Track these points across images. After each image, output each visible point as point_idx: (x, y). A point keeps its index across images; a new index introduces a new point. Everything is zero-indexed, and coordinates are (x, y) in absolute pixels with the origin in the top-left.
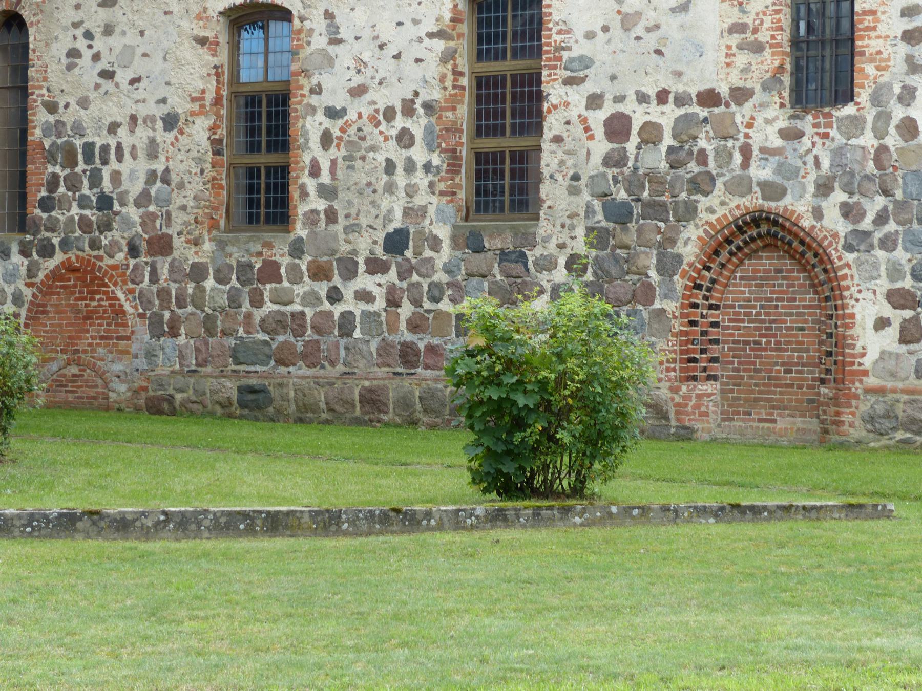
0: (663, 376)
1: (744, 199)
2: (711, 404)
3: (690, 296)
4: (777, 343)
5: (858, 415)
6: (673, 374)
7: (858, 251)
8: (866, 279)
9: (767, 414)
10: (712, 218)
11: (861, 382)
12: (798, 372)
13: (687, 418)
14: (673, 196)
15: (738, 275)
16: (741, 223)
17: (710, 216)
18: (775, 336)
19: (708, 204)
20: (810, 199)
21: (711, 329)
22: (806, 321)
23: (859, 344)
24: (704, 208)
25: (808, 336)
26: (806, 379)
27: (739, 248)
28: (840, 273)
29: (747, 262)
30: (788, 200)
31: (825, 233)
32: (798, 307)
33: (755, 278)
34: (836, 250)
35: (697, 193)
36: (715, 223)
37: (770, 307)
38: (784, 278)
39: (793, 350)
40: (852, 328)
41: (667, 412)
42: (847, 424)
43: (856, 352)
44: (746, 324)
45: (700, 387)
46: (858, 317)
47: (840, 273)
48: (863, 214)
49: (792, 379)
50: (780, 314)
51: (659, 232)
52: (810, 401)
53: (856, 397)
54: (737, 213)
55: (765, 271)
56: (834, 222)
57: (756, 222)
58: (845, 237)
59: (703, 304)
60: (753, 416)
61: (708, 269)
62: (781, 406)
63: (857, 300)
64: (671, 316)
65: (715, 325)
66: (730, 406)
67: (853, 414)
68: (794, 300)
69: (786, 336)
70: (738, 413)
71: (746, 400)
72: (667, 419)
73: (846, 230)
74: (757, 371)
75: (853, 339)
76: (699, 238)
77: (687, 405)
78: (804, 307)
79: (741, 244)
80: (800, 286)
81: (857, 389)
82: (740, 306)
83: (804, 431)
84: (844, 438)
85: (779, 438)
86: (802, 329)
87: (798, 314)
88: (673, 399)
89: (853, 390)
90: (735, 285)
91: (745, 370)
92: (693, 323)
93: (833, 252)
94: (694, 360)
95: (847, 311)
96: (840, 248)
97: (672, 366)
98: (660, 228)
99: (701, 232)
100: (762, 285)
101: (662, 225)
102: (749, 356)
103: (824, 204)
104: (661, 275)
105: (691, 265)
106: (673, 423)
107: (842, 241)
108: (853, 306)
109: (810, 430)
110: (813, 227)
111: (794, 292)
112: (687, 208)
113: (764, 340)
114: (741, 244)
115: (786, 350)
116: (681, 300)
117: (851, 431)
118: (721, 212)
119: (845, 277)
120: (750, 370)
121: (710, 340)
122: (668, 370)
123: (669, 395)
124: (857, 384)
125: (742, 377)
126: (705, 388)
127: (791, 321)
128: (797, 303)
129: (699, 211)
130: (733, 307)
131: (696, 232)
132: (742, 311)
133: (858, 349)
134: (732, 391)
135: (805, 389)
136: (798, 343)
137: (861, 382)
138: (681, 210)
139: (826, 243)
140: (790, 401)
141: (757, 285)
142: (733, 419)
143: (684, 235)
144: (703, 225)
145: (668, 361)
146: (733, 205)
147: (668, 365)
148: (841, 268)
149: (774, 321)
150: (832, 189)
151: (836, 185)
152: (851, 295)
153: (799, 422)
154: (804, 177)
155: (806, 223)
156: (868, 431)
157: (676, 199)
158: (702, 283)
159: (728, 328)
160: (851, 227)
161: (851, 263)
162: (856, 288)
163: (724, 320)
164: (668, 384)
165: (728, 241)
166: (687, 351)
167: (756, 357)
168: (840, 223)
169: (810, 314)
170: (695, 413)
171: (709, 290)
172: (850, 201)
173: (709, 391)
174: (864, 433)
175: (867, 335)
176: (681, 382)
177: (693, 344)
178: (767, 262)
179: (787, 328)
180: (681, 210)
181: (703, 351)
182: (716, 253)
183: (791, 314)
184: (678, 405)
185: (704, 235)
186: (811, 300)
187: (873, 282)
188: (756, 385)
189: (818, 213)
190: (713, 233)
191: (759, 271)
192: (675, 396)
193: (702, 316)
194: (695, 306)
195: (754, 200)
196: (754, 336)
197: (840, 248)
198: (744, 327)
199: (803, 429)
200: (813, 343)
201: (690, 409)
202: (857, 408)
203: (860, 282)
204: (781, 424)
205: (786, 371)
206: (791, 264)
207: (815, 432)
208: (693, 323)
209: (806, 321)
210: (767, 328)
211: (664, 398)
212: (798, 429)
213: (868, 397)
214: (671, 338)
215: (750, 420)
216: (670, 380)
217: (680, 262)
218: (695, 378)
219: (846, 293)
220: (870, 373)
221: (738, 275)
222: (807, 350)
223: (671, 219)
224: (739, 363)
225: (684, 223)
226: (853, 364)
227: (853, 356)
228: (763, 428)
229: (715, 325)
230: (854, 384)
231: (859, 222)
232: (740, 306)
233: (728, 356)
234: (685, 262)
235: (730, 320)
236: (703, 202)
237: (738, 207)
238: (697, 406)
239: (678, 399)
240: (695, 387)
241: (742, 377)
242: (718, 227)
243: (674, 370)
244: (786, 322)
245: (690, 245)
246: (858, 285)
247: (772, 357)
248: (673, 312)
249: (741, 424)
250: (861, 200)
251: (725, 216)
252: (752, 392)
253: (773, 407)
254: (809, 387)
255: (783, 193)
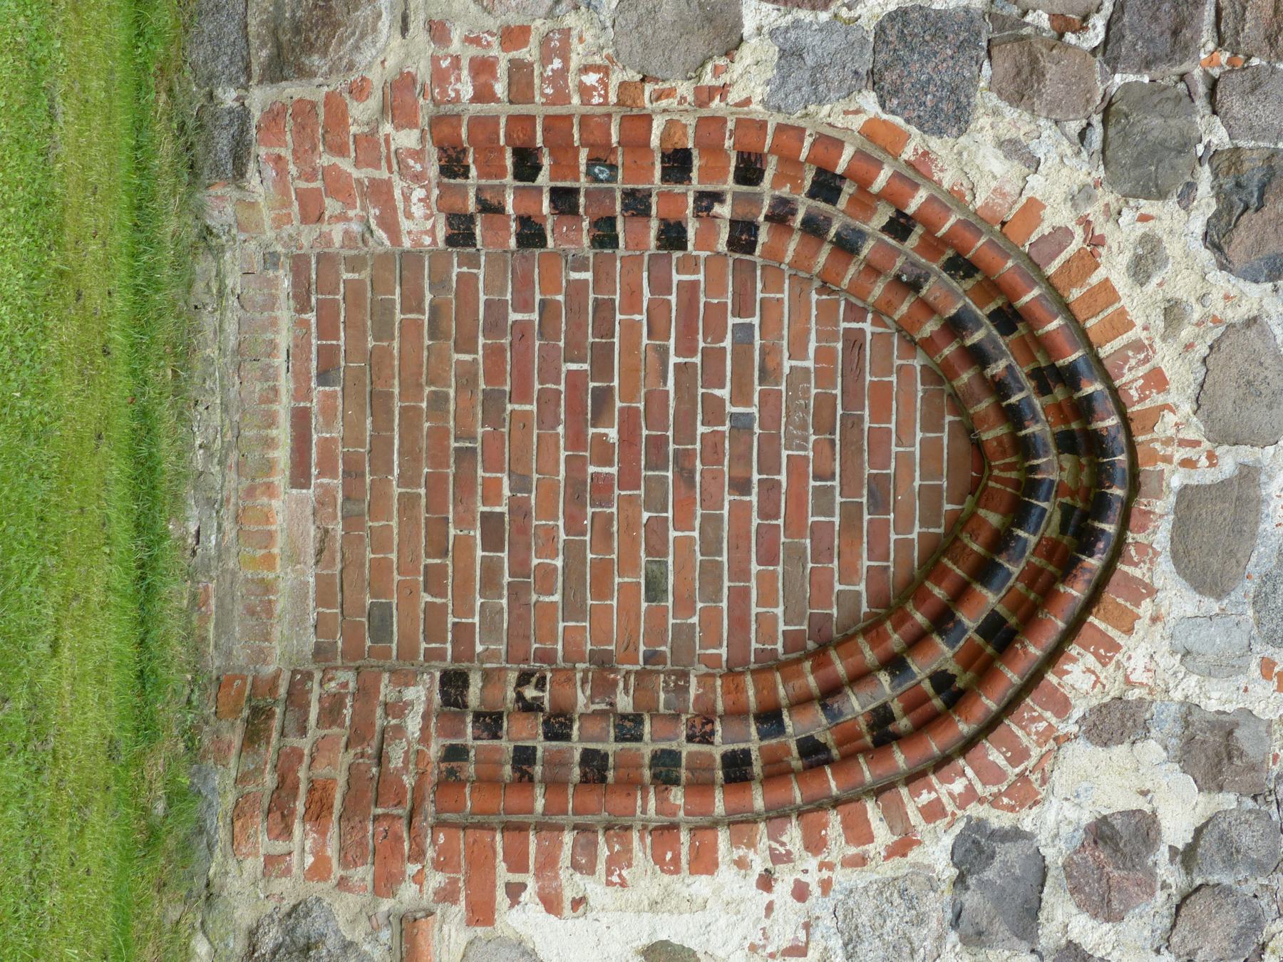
0: (456, 46)
1: (1187, 408)
2: (356, 227)
3: (789, 161)
4: (602, 488)
5: (318, 888)
6: (467, 91)
7: (960, 882)
8: (849, 914)
9: (326, 444)
10: (1113, 268)
11: (447, 895)
12: (491, 570)
13: (287, 153)
14: (1213, 85)
15: (868, 327)
16: (1088, 389)
17: (1125, 259)
18: (629, 478)
19: (1173, 248)
20: (1178, 695)
21: (654, 225)
22: (684, 605)
23: (593, 887)
24: (1158, 228)
25: (629, 610)
26: (464, 606)
27: (978, 357)
28: (872, 810)
29: (917, 363)
30: (1176, 598)
31: (1035, 752)
32: (740, 572)
33: (852, 395)
34: (970, 795)
35: (1218, 192)
36: (1095, 279)
37: (741, 458)
38: (851, 515)
39: (574, 553)
40: (659, 860)
41: (303, 73)
42: (280, 847)
43: (564, 874)
44: (673, 360)
45: (419, 193)
46: (701, 885)
47: (872, 810)
48: (1105, 907)
49: (464, 545)
50: (711, 501)
51: (1063, 25)
52: (380, 623)
53: (386, 884)
54: (1131, 378)
55: (879, 440)
56: (1081, 785)
57: (1084, 443)
58: (1015, 835)
59: (756, 200)
60: (317, 391)
61: (900, 226)
62: (358, 505)
63: (766, 882)
64: (708, 79)
65: (673, 236)
66: (355, 290)
67: (319, 871)
68: (768, 558)
69: (630, 525)
70: (327, 329)
71: (377, 361)
72: (278, 70)
73: (1043, 838)
74: (493, 401)
75: (612, 862)
76: (1033, 209)
77: (341, 151)
78: (740, 597)
79: (998, 368)
80: (820, 583)
81: (419, 879)
82: (744, 332)
83: (261, 611)
84: (222, 835)
85: (228, 513)
86: (655, 589)
87: (711, 573)
88: (359, 90)
89: (412, 868)
90: (827, 313)
91: (494, 354)
92: (677, 164)
93: (958, 786)
94: (526, 165)
95: (723, 836)
96: (975, 810)
97: (500, 88)
98: (1082, 25)
99: (1057, 215)
100: (823, 426)
101: (1096, 34)
102: (549, 373)
103: (1151, 750)
104: (881, 30)
105: (919, 170)
106: (260, 98)
107: (999, 819)
108: (741, 864)
109: (266, 637)
110: (1062, 706)
111: (796, 555)
112: (1156, 152)
113: (613, 434)
114: (998, 368)
115: (573, 525)
116: (773, 121)
117: (253, 865)
118: (1139, 304)
119: (858, 832)
120: (494, 374)
121: (611, 221)
122: (483, 68)
123: (376, 77)
124: (436, 880)
125: (466, 344)
126: (418, 210)
127: (684, 545)
128: (755, 568)
129: (1147, 206)
130: (743, 307)
131: (1059, 193)
132: (727, 343)
133: (571, 883)
134: (412, 302)
135: (427, 598)
136: (603, 571)
137: (447, 895)
138: (1154, 125)
139: (996, 756)
140: (381, 543)
141: (825, 402)
142: (303, 306)
143: (1050, 142)
144: (1086, 223)
145: (519, 70)
146: (1166, 357)
147: (502, 69)
148: (895, 817)
149: (685, 475)
150: (1211, 781)
151: (1228, 800)
152: (787, 858)
153: (292, 578)
154: (1267, 667)
155: (1079, 677)
156: (252, 933)
157: (1201, 103)
158: (843, 202)
159: (659, 285)
160: (1054, 855)
161: (914, 855)
162: (813, 879)
163: (690, 265)
164: (422, 71)
165: (1008, 319)
166: (563, 150)
167: (547, 400)
168: (1071, 813)
169: (710, 618)
170: (311, 177)
171: (814, 227)
172: (1163, 854)
173: (405, 225)
174: (244, 916)
175: (629, 916)
176: (436, 121)
177: (592, 162)
178: (915, 447)
179: (657, 530)
180: (1154, 125)
181: (564, 199)
182: (961, 266)
183: (711, 546)
184: (337, 113)
185: (1045, 229)
186: (766, 622)
187: (836, 943)
188: (438, 401)
189: (1116, 723)
190: (1051, 270)
191: (881, 412)
192: (374, 103)
193: (708, 200)
194: (749, 172)
195: (1180, 454)
196: (629, 395)
197: (975, 810)
198: (664, 352)
199: (269, 608)
200: (601, 635)
201: (325, 160)
202: (343, 884)
203: (837, 895)
204: (287, 509)
205: (491, 524)
206: (904, 545)
207: (260, 656)
208: (677, 164)
209: (684, 605)
210: (658, 444)
211: (363, 58)
212: (267, 587)
213: (385, 935)
214: (616, 78)
215: (300, 377)
216: (440, 77)
217: (934, 123)
218: (453, 166)
219: (793, 835)
220: (480, 931)
221: (868, 327)
222: (573, 608)
223: (1118, 79)
224: (522, 330)
225: (1096, 135)
226: (517, 863)
227: (548, 863)
228: (269, 443)
229: (673, 236)
230: (439, 866)
231: (1075, 890)
232: (744, 332)
233: (550, 283)
234: (934, 143)
235: (690, 290)
236: (1182, 225)
237: (1157, 380)
238: (337, 185)
239: (360, 112)
240: (417, 178)
241: (466, 344)
242: (1075, 294)
243: (484, 94)
244: (683, 521)
245: (1009, 164)
246: (826, 886)
247: (548, 467)
248: (724, 90)
249: (284, 340)
250: (1161, 896)
251: (1122, 323)
252: (411, 388)
253: (353, 473)
254: (434, 614)
255: (1206, 578)
